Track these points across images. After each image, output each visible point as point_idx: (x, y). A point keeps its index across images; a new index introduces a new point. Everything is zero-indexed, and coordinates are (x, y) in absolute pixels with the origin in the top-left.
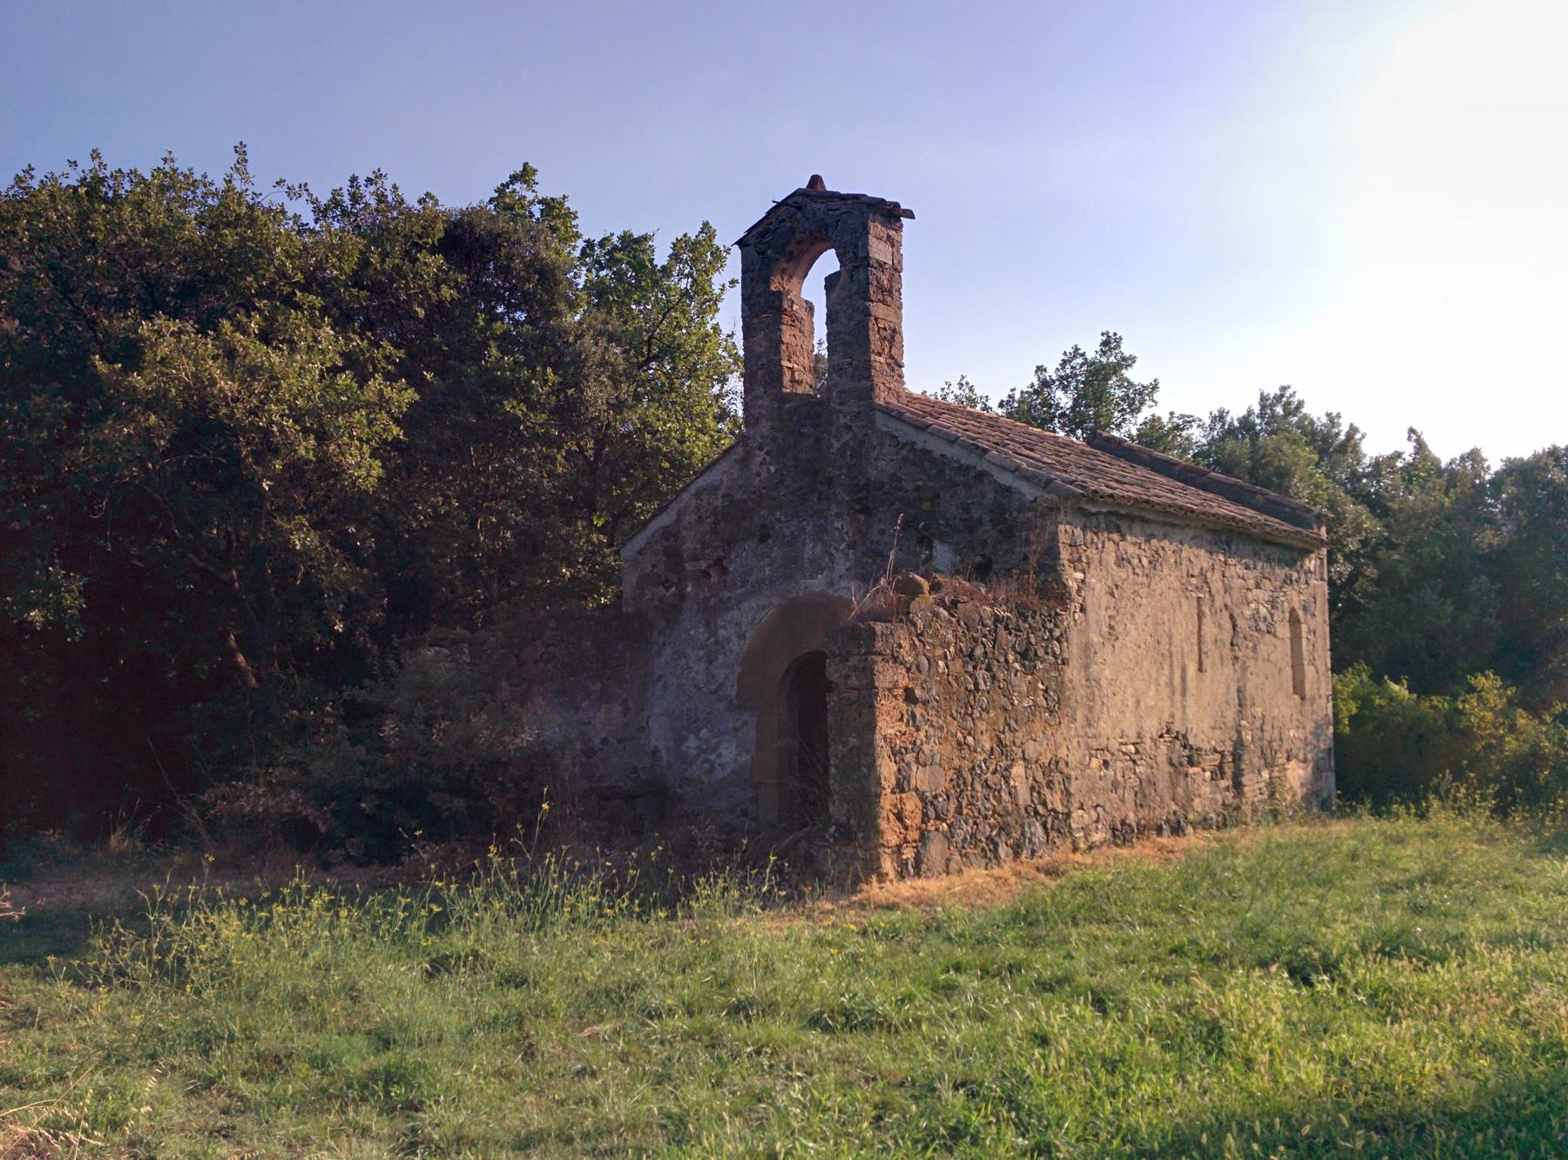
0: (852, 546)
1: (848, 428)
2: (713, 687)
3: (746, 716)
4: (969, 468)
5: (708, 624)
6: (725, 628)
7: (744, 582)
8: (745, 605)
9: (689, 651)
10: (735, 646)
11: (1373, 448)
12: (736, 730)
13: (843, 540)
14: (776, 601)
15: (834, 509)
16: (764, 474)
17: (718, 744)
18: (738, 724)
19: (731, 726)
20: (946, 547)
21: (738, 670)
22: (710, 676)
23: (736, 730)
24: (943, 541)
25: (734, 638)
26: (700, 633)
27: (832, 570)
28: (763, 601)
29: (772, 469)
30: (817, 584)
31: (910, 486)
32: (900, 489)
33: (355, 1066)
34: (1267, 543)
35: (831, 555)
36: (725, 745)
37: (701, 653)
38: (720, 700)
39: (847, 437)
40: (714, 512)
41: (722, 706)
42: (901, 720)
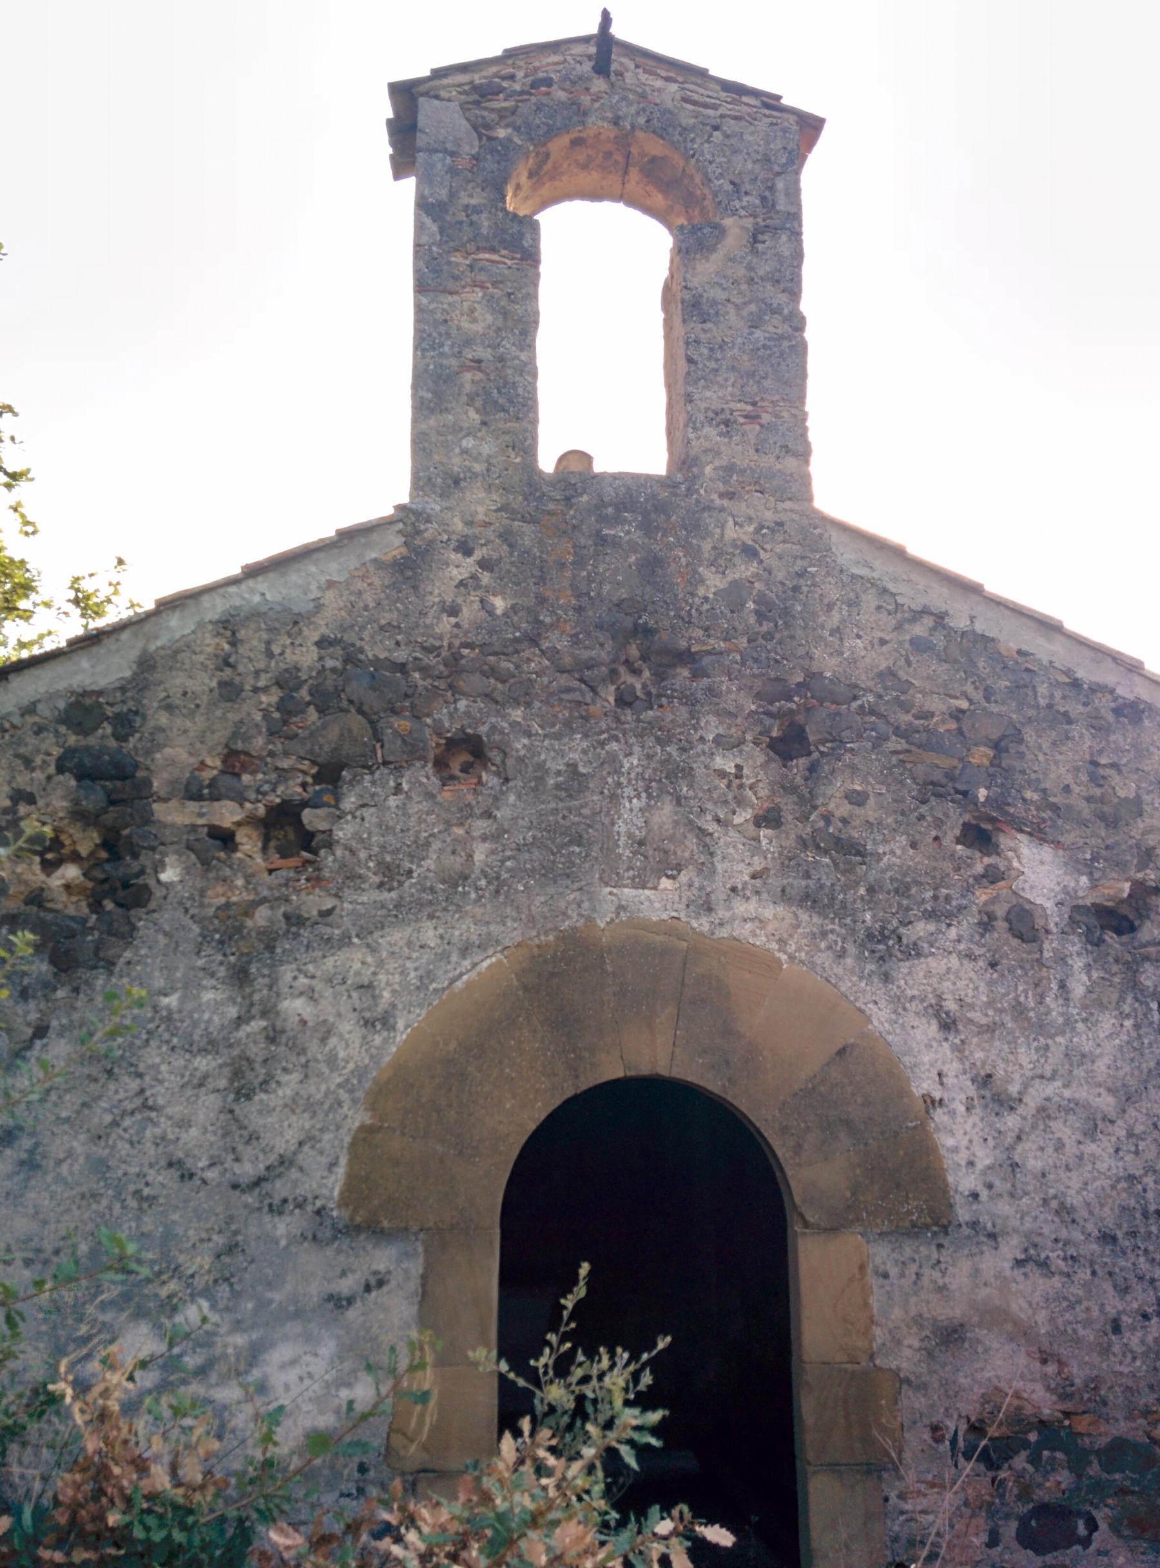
0: (769, 819)
1: (750, 552)
2: (247, 1170)
3: (382, 1258)
4: (1097, 689)
5: (240, 976)
6: (311, 995)
7: (390, 875)
8: (396, 937)
9: (152, 1056)
10: (350, 1045)
11: (598, 468)
12: (339, 1302)
13: (741, 802)
14: (512, 933)
15: (712, 727)
16: (470, 613)
17: (254, 1354)
18: (346, 1285)
19: (315, 1290)
20: (1047, 853)
21: (356, 1117)
22: (236, 1132)
23: (339, 1302)
24: (1039, 834)
25: (348, 1027)
26: (214, 1003)
27: (706, 870)
28: (465, 929)
29: (499, 604)
30: (658, 902)
31: (936, 704)
32: (905, 707)
33: (1114, 1307)
34: (355, 1426)
35: (703, 833)
36: (282, 1353)
37: (203, 1063)
38: (278, 1210)
39: (744, 570)
40: (287, 681)
41: (283, 1228)
42: (595, 1402)
